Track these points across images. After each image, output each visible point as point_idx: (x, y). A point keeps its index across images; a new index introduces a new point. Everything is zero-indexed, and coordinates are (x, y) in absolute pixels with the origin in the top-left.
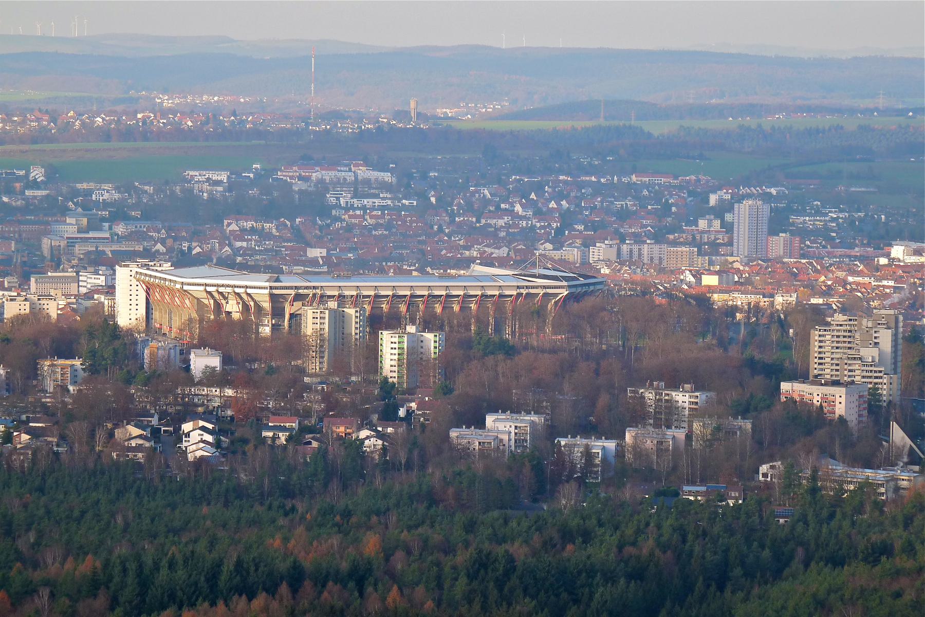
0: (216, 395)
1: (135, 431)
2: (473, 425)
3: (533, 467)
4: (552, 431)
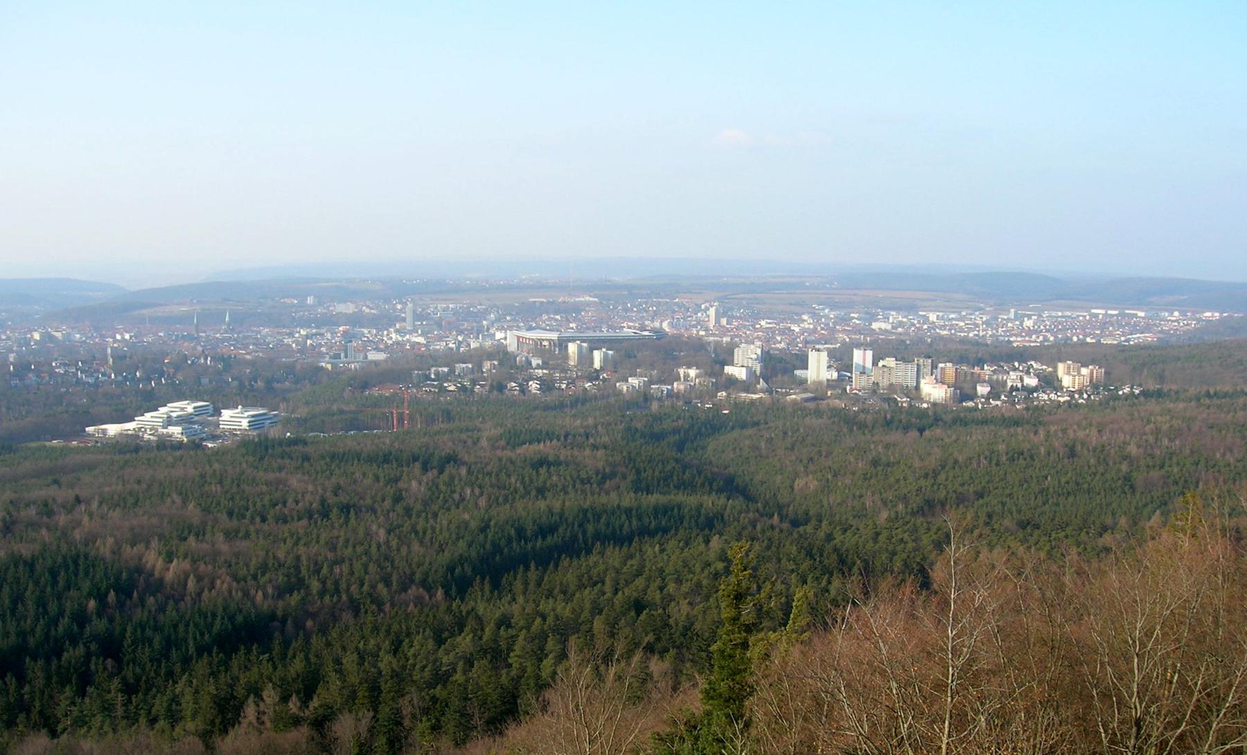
0: (540, 372)
1: (514, 384)
2: (185, 444)
3: (50, 572)
4: (651, 382)
